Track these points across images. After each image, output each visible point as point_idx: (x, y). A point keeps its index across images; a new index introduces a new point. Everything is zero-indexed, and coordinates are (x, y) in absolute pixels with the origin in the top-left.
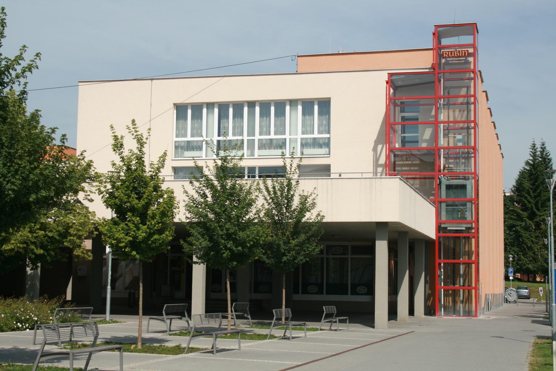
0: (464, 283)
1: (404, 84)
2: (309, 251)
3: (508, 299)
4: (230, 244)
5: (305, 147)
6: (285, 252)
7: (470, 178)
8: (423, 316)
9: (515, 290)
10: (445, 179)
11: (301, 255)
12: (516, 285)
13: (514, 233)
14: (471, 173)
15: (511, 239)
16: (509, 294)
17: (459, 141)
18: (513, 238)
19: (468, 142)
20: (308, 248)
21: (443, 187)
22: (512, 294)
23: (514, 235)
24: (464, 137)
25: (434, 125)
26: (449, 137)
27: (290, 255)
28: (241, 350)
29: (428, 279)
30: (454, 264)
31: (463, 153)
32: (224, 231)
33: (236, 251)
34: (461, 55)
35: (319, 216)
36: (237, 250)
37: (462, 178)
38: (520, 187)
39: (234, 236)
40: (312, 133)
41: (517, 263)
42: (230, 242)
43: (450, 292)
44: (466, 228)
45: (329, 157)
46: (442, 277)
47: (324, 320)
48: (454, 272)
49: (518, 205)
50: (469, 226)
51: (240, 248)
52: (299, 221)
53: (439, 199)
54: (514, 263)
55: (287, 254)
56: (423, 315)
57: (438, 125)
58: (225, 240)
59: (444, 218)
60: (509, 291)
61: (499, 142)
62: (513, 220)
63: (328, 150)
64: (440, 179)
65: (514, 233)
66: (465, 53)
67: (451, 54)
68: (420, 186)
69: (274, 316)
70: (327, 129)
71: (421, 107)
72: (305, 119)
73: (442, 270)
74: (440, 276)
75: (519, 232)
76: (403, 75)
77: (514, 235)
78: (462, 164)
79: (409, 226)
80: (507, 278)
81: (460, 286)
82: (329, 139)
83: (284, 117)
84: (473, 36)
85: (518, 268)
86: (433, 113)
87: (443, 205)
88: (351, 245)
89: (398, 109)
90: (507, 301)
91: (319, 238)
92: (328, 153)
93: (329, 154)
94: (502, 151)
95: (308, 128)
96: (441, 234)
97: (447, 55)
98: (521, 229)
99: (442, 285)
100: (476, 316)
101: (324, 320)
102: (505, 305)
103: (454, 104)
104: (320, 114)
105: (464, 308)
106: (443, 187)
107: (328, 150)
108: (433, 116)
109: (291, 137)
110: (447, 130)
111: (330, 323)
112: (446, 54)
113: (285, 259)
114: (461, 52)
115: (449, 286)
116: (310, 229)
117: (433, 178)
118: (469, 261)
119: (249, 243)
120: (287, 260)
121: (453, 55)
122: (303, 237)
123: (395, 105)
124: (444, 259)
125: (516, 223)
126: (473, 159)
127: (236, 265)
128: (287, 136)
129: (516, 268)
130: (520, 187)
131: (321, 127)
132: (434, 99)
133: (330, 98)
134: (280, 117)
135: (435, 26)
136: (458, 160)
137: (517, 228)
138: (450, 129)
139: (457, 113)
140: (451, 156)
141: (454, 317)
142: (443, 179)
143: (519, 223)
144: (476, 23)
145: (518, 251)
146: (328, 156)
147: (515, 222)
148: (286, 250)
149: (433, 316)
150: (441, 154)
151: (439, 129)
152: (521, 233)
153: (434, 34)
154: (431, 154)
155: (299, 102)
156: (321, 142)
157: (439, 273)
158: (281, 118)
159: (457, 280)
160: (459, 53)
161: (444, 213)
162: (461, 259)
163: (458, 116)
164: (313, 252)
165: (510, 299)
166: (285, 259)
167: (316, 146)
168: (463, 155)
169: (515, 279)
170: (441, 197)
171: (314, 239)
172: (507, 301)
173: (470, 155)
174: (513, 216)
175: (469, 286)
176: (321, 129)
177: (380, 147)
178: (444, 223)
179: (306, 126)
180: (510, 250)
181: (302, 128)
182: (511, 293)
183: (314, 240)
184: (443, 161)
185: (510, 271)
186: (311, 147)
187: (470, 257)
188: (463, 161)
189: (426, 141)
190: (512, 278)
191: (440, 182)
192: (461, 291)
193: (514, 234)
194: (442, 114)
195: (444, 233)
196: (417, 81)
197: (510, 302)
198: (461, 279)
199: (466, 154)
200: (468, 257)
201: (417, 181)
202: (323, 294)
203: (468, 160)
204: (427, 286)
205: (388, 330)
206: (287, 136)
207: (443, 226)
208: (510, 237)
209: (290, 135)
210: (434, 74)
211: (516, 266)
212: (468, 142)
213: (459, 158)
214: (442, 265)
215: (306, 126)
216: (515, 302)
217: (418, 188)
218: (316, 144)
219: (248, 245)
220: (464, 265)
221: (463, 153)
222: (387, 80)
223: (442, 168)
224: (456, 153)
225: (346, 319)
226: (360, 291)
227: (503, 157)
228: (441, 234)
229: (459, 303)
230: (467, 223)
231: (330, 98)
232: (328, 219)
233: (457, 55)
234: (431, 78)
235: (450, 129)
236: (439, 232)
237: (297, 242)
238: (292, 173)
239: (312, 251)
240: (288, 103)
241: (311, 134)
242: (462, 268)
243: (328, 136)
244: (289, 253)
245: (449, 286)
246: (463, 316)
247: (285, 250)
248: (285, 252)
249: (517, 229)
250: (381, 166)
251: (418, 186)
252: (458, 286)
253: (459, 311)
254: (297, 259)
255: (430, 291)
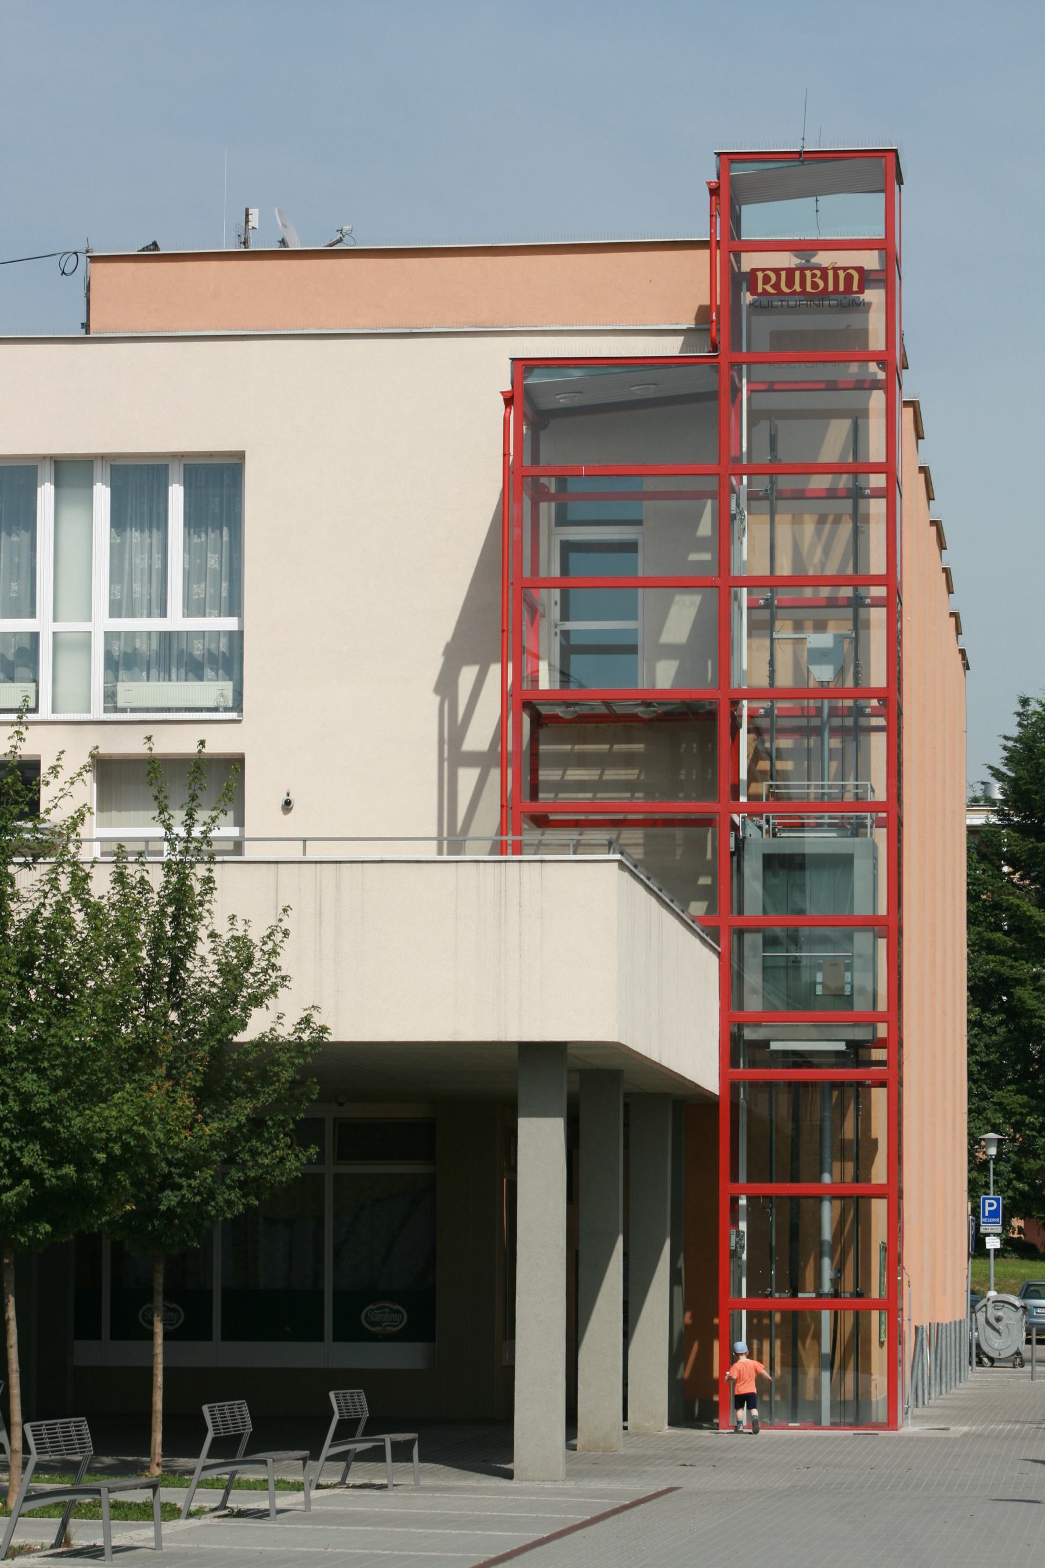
0: (836, 1282)
1: (585, 403)
2: (261, 1166)
3: (985, 1348)
4: (31, 1156)
5: (122, 674)
6: (170, 1172)
7: (869, 822)
8: (667, 1430)
9: (1017, 1302)
10: (760, 828)
11: (228, 1181)
12: (1012, 1276)
13: (1001, 1017)
14: (876, 807)
15: (986, 1046)
16: (988, 1322)
17: (819, 656)
18: (998, 1046)
19: (856, 658)
20: (254, 1153)
21: (753, 866)
22: (1005, 1321)
23: (1002, 1030)
24: (839, 639)
25: (715, 590)
26: (776, 642)
27: (193, 1183)
28: (165, 1550)
29: (681, 1263)
30: (795, 1201)
31: (834, 712)
32: (12, 1103)
33: (54, 1180)
34: (831, 288)
35: (308, 1027)
36: (58, 1178)
37: (830, 825)
38: (1034, 788)
39: (47, 1124)
40: (156, 611)
41: (1016, 1169)
42: (31, 1146)
43: (777, 1317)
44: (850, 1043)
45: (239, 721)
46: (744, 1257)
47: (331, 1446)
48: (794, 1233)
49: (1022, 878)
50: (860, 1034)
51: (69, 1170)
52: (225, 1046)
53: (736, 920)
54: (1003, 1167)
55: (177, 1179)
56: (667, 1427)
57: (729, 592)
58: (14, 1139)
59: (753, 1003)
60: (990, 1310)
61: (955, 603)
62: (999, 953)
63: (228, 686)
64: (734, 827)
65: (1001, 1017)
66: (849, 278)
67: (790, 283)
68: (646, 853)
69: (206, 1430)
70: (224, 594)
71: (647, 504)
72: (122, 545)
73: (743, 1226)
74: (735, 1254)
75: (1030, 1014)
76: (576, 366)
77: (1002, 1030)
78: (830, 759)
79: (644, 1053)
80: (977, 1248)
81: (820, 1295)
82: (236, 638)
83: (25, 536)
84: (883, 195)
85: (1022, 1193)
86: (705, 528)
87: (753, 941)
88: (335, 1119)
89: (548, 511)
90: (980, 1357)
91: (302, 1115)
92: (230, 704)
93: (238, 706)
94: (964, 641)
95: (137, 587)
96: (744, 1072)
97: (772, 286)
98: (1037, 998)
99: (744, 1296)
100: (891, 1423)
101: (331, 1446)
102: (977, 1377)
103: (800, 495)
104: (193, 521)
105: (837, 1387)
106: (753, 866)
107: (228, 686)
108: (704, 539)
109: (61, 627)
110: (768, 611)
111: (343, 1464)
112: (766, 280)
113: (169, 1199)
114: (831, 273)
115: (771, 1295)
116: (265, 1078)
117: (708, 823)
118: (860, 1188)
119: (104, 1149)
120: (180, 1203)
121: (797, 287)
122: (243, 1109)
123: (539, 495)
124: (750, 1179)
125: (1012, 967)
126: (878, 743)
127: (46, 1233)
128: (43, 624)
129: (1010, 1193)
130: (1034, 788)
131: (199, 583)
132: (716, 479)
133: (241, 455)
134: (9, 534)
135: (719, 154)
136: (813, 741)
137: (1019, 992)
138: (778, 607)
139: (809, 528)
140: (783, 723)
141: (794, 1433)
142: (751, 832)
143: (1026, 967)
144: (895, 151)
145: (1022, 1106)
146: (233, 715)
147: (1010, 962)
148: (178, 1164)
149: (701, 1428)
150: (741, 716)
151: (735, 606)
152: (1036, 1021)
153: (714, 192)
154: (696, 714)
155: (98, 469)
156: (198, 649)
157: (733, 1243)
158: (15, 538)
159: (805, 1267)
160: (824, 277)
161: (753, 978)
162: (827, 1178)
163: (813, 547)
164: (277, 1172)
165: (996, 1345)
166: (169, 1199)
167: (174, 671)
168: (836, 722)
169: (1012, 1247)
170: (741, 911)
171: (282, 1118)
172: (980, 1357)
173: (863, 721)
174: (1000, 935)
175: (859, 1295)
176: (198, 590)
177: (468, 675)
178: (757, 1023)
179: (126, 577)
180: (985, 1104)
181: (111, 584)
182: (998, 1319)
183: (282, 1124)
184: (749, 744)
185: (987, 1208)
186: (154, 672)
187: (862, 1172)
188: (835, 743)
189: (670, 651)
190: (998, 1246)
191: (740, 843)
192: (826, 1316)
193: (1001, 1023)
194: (745, 540)
195: (752, 1064)
196: (638, 392)
197: (992, 1360)
198: (826, 1262)
199: (849, 716)
200: (857, 1168)
201: (634, 836)
202: (209, 1338)
203: (856, 740)
204: (679, 1291)
205: (570, 1485)
206: (43, 624)
207: (749, 1034)
208: (986, 1038)
209: (55, 620)
210: (717, 368)
211: (1010, 1181)
212: (856, 658)
213: (818, 731)
214: (743, 1202)
215: (126, 577)
216: (1018, 1359)
217: (639, 860)
218: (174, 659)
219: (101, 1157)
220: (838, 1203)
221: (834, 712)
222: (509, 388)
223: (743, 775)
224: (804, 713)
225: (410, 1443)
226: (379, 1324)
227: (967, 667)
228: (744, 1072)
229: (811, 1372)
230: (856, 1024)
231: (241, 455)
232: (332, 1037)
233: (815, 285)
234: (702, 380)
235: (778, 607)
236: (735, 1064)
237: (219, 1130)
238: (192, 846)
239: (274, 1167)
240: (46, 471)
241: (150, 615)
242: (828, 1213)
243: (230, 624)
244: (189, 1176)
245: (771, 1295)
246: (834, 1426)
247: (170, 1163)
248: (170, 1172)
249: (1020, 999)
250: (473, 759)
251: (638, 853)
252: (813, 1295)
253: (817, 1404)
254: (214, 1199)
255: (688, 1315)
